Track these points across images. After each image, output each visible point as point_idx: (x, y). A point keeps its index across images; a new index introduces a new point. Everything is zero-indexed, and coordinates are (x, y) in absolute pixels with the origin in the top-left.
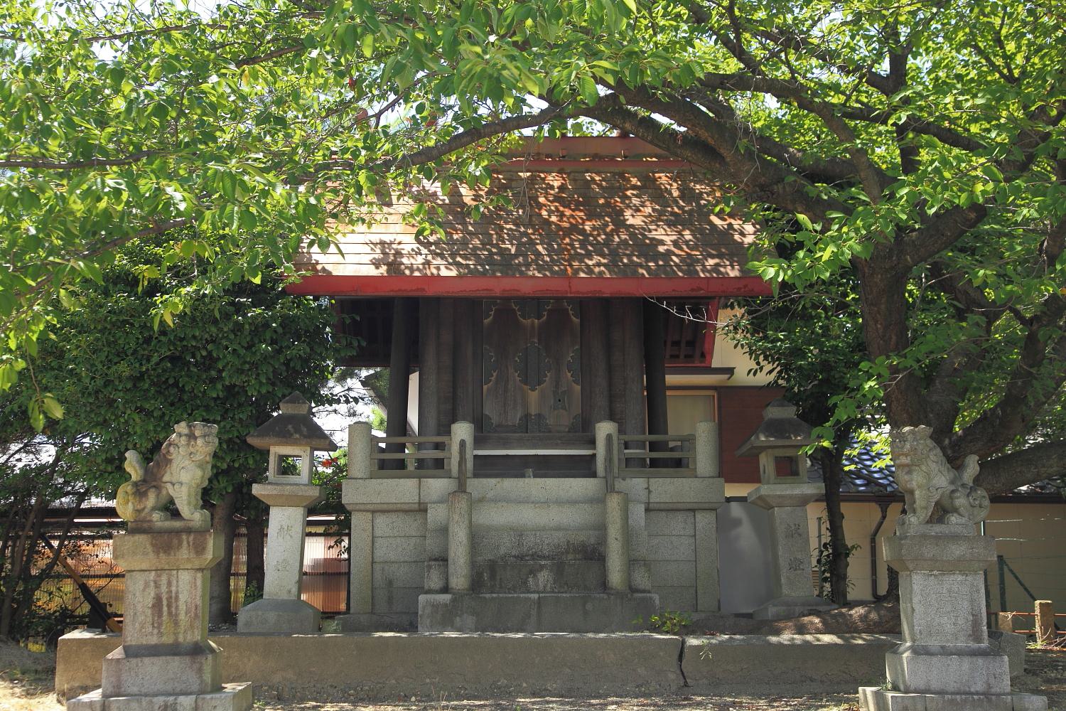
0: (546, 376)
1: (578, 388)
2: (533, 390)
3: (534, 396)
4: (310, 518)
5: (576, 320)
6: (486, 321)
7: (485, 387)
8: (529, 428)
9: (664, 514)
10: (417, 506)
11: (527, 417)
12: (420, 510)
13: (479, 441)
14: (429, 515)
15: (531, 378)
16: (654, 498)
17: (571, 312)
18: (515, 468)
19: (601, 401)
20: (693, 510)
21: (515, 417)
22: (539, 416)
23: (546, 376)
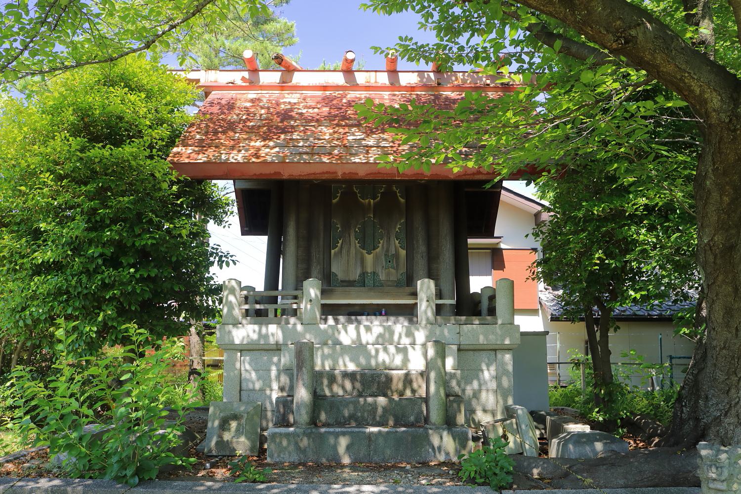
0: (380, 243)
1: (403, 253)
2: (369, 253)
3: (369, 258)
4: (280, 288)
5: (402, 200)
6: (334, 201)
7: (333, 251)
8: (362, 283)
9: (472, 352)
10: (275, 346)
11: (363, 274)
12: (278, 350)
13: (324, 292)
14: (146, 50)
15: (367, 244)
16: (464, 341)
17: (398, 194)
18: (354, 312)
19: (421, 263)
20: (495, 350)
21: (355, 274)
22: (374, 273)
23: (380, 243)
